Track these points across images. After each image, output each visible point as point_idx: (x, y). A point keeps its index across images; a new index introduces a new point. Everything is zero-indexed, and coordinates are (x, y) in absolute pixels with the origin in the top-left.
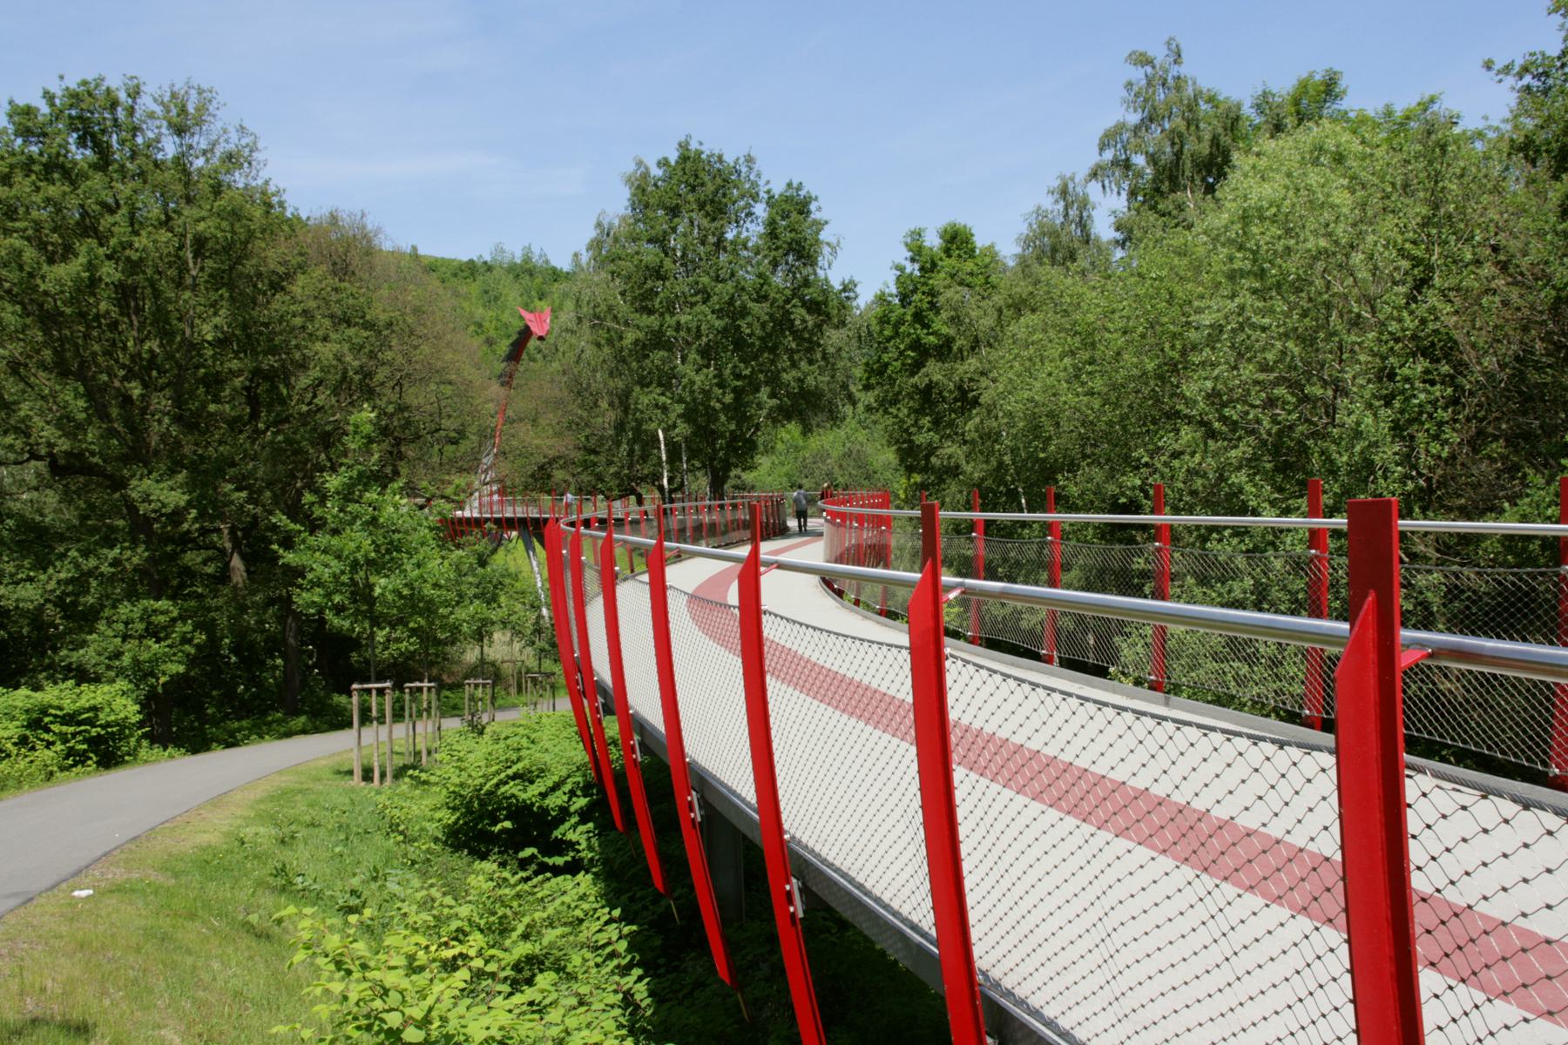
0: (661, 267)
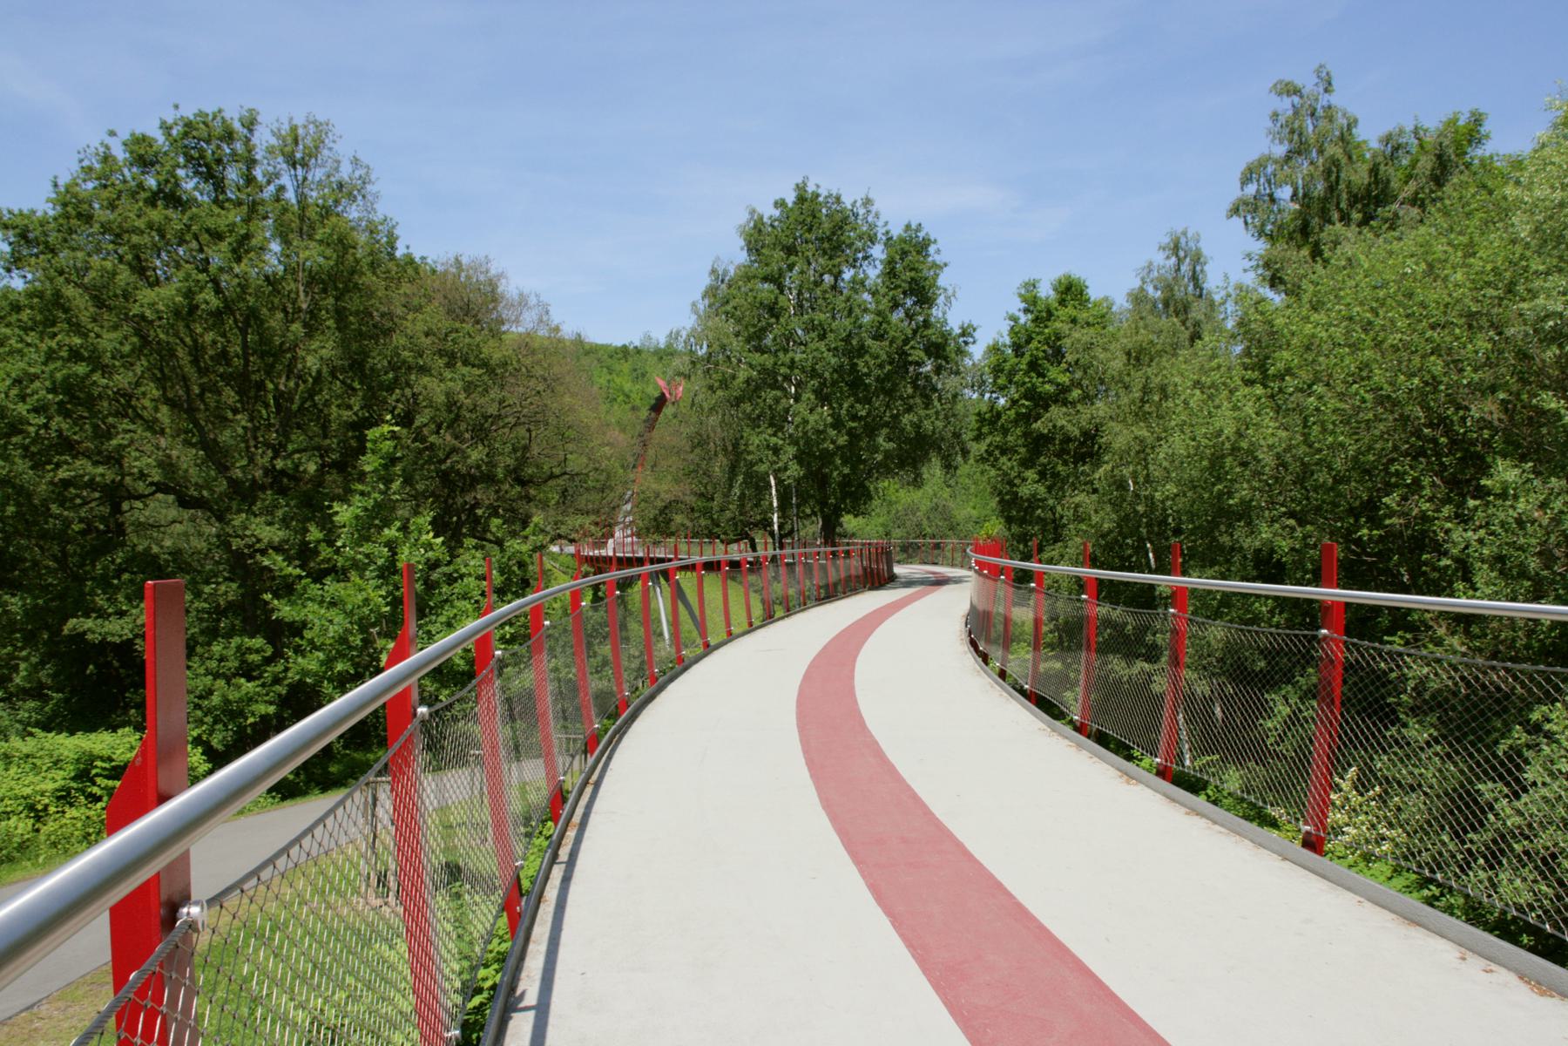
0: (776, 303)
